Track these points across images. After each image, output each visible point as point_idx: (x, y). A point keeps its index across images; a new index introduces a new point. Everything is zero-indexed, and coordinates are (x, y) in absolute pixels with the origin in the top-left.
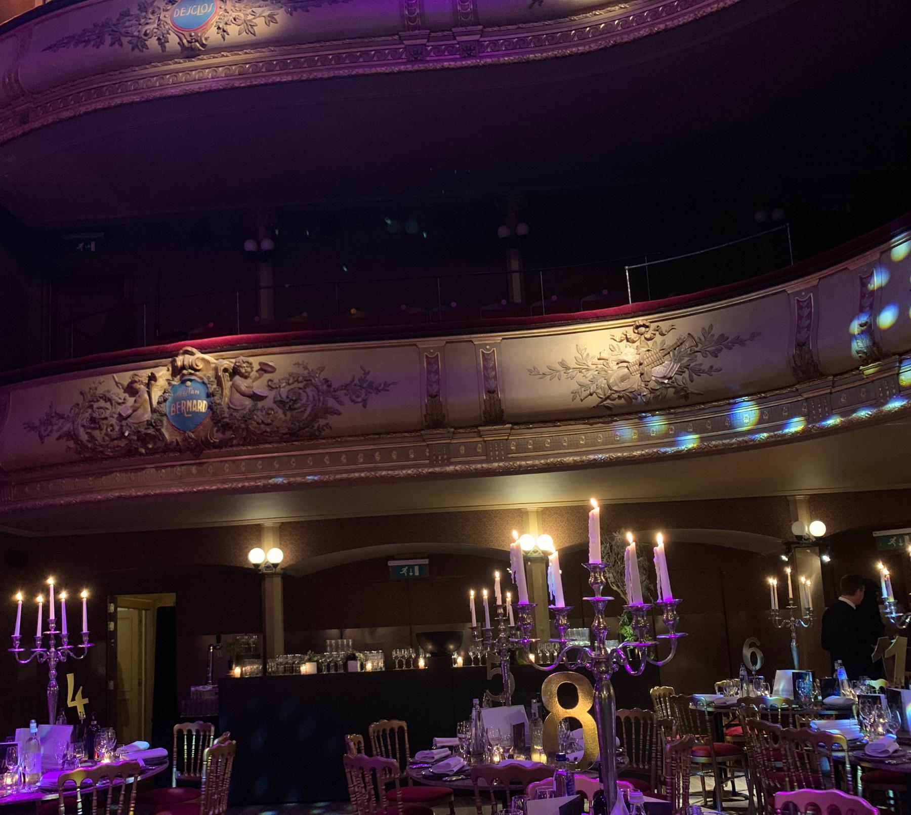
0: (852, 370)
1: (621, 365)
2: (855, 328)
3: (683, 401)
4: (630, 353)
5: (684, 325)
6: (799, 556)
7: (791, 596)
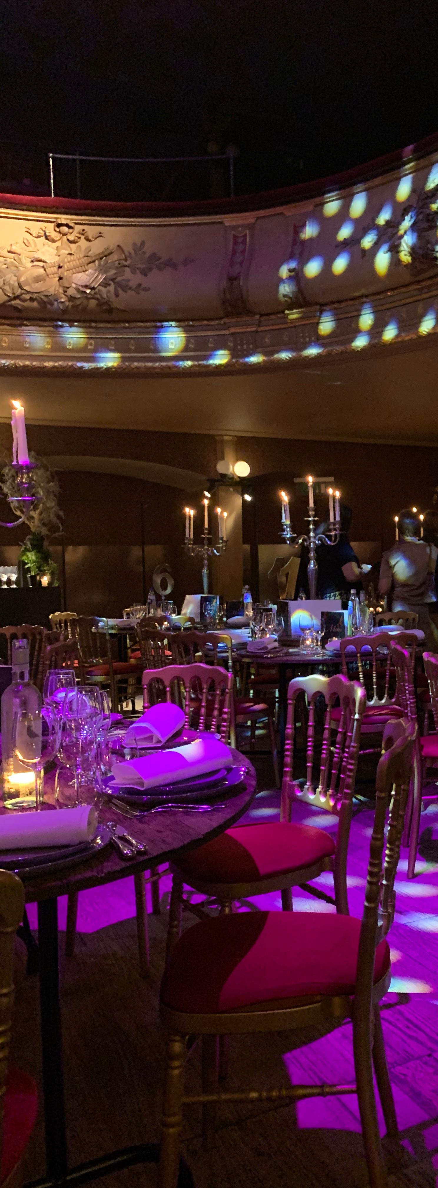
0: (278, 313)
1: (36, 263)
2: (284, 272)
3: (105, 316)
4: (49, 253)
5: (113, 234)
6: (222, 493)
7: (206, 526)
